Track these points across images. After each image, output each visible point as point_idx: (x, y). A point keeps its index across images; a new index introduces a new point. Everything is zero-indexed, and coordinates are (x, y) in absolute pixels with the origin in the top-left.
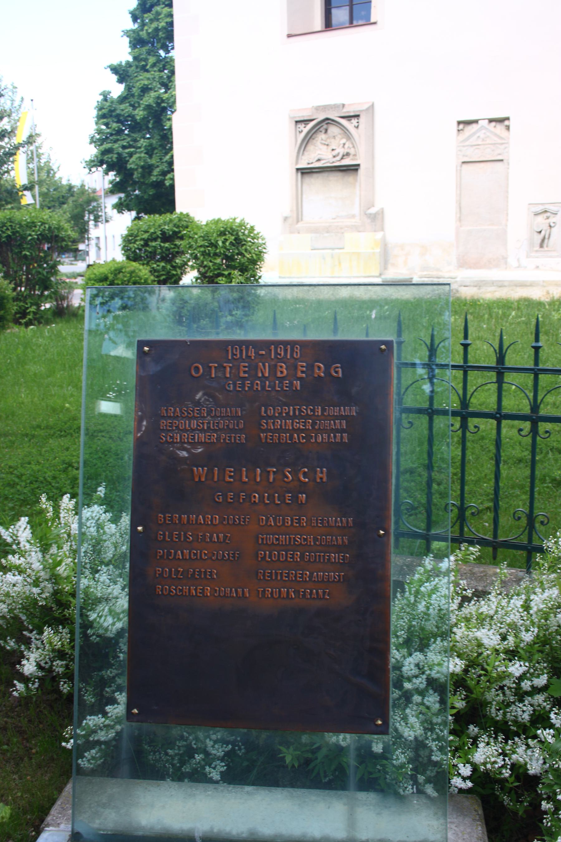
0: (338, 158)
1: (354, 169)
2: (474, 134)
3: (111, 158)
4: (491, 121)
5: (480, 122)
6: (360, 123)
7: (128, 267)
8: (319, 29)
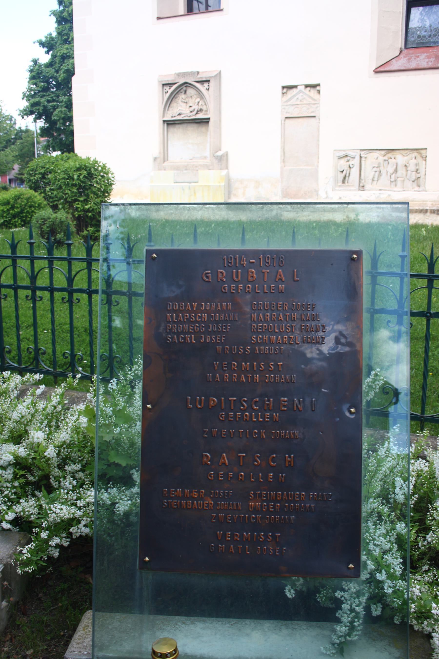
0: (194, 113)
1: (205, 122)
2: (294, 96)
3: (39, 109)
4: (307, 86)
5: (298, 87)
6: (210, 86)
7: (27, 194)
8: (182, 13)
